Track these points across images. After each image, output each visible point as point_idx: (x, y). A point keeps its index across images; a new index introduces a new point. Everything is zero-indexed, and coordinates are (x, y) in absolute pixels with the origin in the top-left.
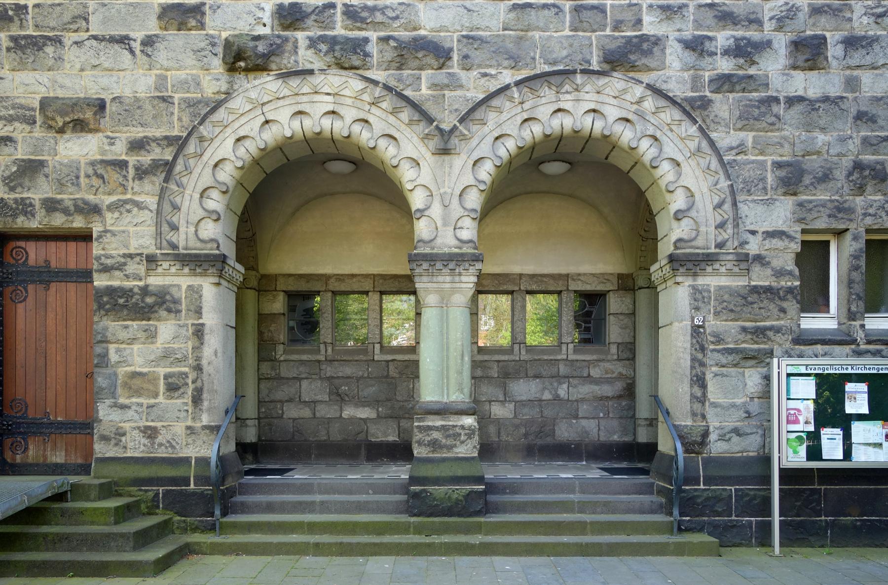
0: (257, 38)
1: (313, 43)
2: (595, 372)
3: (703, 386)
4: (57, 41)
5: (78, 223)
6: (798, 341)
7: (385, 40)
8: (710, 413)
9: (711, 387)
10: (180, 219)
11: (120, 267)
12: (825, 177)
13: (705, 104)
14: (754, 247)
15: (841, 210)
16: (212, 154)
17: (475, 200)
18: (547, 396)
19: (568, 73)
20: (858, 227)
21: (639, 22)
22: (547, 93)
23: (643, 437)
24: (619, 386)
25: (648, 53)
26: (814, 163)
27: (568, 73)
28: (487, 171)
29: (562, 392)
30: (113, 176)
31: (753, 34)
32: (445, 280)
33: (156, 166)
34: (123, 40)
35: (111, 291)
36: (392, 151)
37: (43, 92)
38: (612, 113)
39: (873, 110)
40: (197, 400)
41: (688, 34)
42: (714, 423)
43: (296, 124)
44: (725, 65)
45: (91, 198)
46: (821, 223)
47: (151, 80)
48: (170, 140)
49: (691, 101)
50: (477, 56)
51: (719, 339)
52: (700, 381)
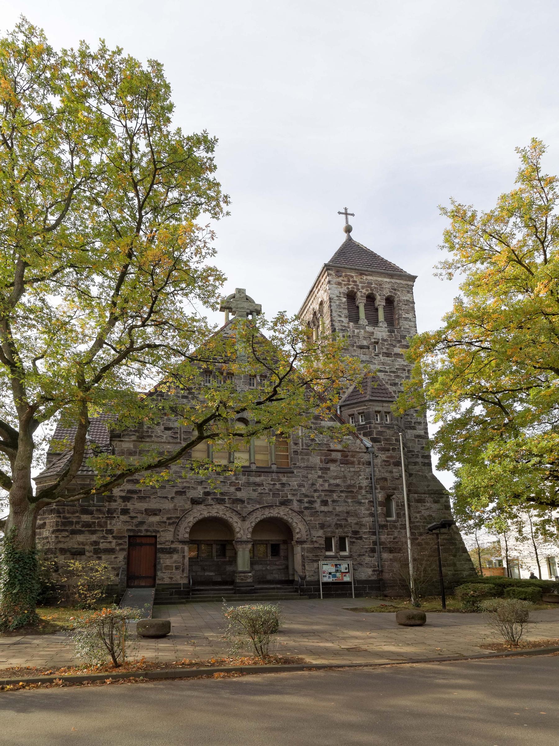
0: (200, 498)
1: (212, 499)
2: (277, 563)
3: (305, 566)
4: (149, 497)
5: (154, 534)
6: (325, 557)
7: (230, 499)
8: (306, 572)
9: (306, 566)
10: (180, 534)
11: (164, 543)
12: (329, 526)
13: (302, 512)
14: (314, 539)
15: (333, 532)
16: (187, 520)
17: (251, 530)
18: (264, 569)
19: (272, 506)
20: (337, 536)
21: (287, 497)
22: (267, 510)
23: (291, 578)
24: (284, 566)
25: (289, 502)
26: (327, 523)
27: (272, 506)
28: (253, 524)
29: (268, 568)
30: (163, 525)
31: (312, 499)
32: (244, 546)
33: (173, 523)
34: (166, 498)
35: (161, 548)
36: (231, 520)
37: (146, 507)
38: (282, 513)
39: (340, 514)
40: (183, 571)
41: (298, 499)
42: (307, 574)
43: (208, 514)
44: (307, 505)
45: (157, 529)
46: (329, 535)
47: (173, 505)
48: (178, 518)
49: (299, 512)
50: (250, 502)
51: (308, 557)
52: (304, 566)
